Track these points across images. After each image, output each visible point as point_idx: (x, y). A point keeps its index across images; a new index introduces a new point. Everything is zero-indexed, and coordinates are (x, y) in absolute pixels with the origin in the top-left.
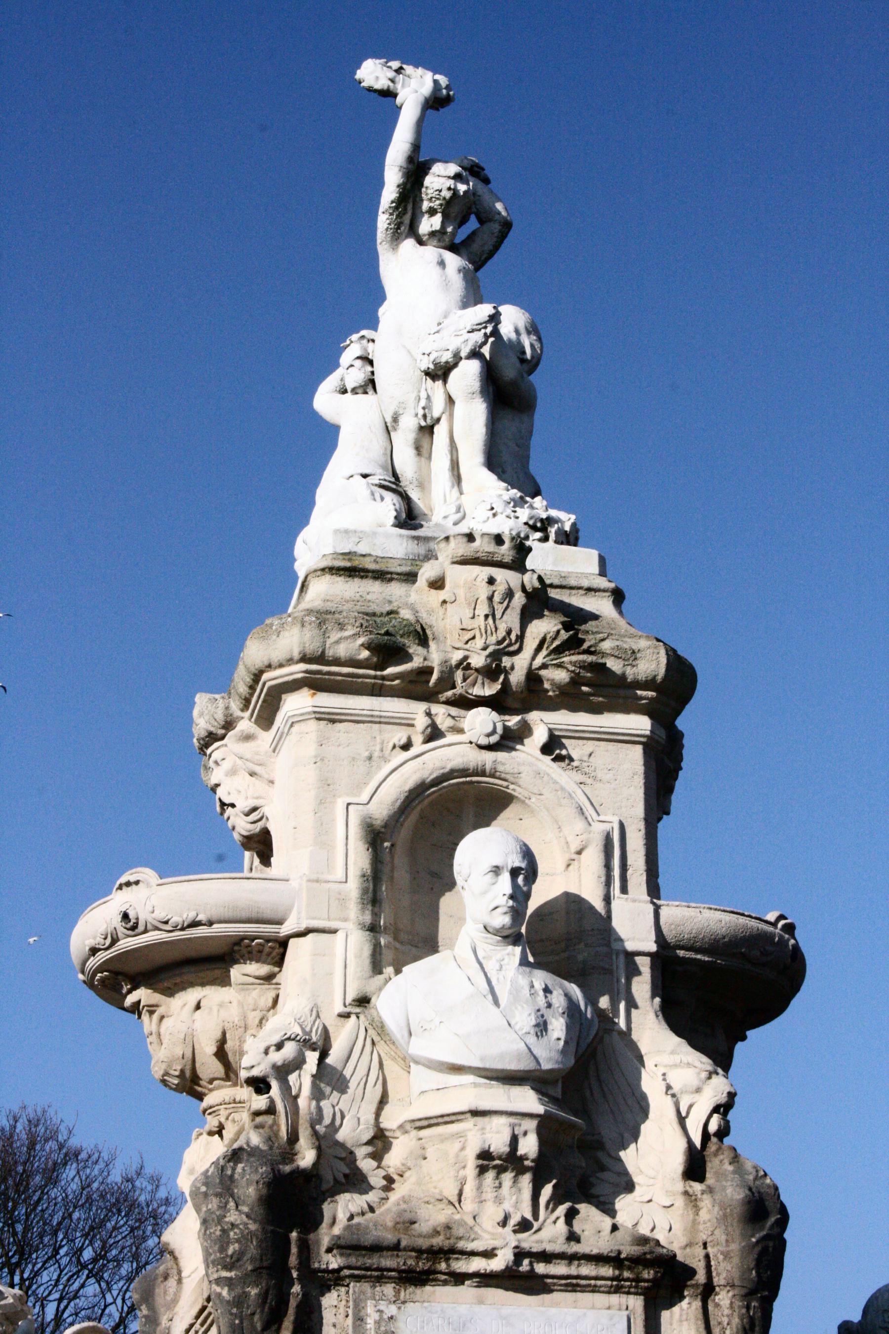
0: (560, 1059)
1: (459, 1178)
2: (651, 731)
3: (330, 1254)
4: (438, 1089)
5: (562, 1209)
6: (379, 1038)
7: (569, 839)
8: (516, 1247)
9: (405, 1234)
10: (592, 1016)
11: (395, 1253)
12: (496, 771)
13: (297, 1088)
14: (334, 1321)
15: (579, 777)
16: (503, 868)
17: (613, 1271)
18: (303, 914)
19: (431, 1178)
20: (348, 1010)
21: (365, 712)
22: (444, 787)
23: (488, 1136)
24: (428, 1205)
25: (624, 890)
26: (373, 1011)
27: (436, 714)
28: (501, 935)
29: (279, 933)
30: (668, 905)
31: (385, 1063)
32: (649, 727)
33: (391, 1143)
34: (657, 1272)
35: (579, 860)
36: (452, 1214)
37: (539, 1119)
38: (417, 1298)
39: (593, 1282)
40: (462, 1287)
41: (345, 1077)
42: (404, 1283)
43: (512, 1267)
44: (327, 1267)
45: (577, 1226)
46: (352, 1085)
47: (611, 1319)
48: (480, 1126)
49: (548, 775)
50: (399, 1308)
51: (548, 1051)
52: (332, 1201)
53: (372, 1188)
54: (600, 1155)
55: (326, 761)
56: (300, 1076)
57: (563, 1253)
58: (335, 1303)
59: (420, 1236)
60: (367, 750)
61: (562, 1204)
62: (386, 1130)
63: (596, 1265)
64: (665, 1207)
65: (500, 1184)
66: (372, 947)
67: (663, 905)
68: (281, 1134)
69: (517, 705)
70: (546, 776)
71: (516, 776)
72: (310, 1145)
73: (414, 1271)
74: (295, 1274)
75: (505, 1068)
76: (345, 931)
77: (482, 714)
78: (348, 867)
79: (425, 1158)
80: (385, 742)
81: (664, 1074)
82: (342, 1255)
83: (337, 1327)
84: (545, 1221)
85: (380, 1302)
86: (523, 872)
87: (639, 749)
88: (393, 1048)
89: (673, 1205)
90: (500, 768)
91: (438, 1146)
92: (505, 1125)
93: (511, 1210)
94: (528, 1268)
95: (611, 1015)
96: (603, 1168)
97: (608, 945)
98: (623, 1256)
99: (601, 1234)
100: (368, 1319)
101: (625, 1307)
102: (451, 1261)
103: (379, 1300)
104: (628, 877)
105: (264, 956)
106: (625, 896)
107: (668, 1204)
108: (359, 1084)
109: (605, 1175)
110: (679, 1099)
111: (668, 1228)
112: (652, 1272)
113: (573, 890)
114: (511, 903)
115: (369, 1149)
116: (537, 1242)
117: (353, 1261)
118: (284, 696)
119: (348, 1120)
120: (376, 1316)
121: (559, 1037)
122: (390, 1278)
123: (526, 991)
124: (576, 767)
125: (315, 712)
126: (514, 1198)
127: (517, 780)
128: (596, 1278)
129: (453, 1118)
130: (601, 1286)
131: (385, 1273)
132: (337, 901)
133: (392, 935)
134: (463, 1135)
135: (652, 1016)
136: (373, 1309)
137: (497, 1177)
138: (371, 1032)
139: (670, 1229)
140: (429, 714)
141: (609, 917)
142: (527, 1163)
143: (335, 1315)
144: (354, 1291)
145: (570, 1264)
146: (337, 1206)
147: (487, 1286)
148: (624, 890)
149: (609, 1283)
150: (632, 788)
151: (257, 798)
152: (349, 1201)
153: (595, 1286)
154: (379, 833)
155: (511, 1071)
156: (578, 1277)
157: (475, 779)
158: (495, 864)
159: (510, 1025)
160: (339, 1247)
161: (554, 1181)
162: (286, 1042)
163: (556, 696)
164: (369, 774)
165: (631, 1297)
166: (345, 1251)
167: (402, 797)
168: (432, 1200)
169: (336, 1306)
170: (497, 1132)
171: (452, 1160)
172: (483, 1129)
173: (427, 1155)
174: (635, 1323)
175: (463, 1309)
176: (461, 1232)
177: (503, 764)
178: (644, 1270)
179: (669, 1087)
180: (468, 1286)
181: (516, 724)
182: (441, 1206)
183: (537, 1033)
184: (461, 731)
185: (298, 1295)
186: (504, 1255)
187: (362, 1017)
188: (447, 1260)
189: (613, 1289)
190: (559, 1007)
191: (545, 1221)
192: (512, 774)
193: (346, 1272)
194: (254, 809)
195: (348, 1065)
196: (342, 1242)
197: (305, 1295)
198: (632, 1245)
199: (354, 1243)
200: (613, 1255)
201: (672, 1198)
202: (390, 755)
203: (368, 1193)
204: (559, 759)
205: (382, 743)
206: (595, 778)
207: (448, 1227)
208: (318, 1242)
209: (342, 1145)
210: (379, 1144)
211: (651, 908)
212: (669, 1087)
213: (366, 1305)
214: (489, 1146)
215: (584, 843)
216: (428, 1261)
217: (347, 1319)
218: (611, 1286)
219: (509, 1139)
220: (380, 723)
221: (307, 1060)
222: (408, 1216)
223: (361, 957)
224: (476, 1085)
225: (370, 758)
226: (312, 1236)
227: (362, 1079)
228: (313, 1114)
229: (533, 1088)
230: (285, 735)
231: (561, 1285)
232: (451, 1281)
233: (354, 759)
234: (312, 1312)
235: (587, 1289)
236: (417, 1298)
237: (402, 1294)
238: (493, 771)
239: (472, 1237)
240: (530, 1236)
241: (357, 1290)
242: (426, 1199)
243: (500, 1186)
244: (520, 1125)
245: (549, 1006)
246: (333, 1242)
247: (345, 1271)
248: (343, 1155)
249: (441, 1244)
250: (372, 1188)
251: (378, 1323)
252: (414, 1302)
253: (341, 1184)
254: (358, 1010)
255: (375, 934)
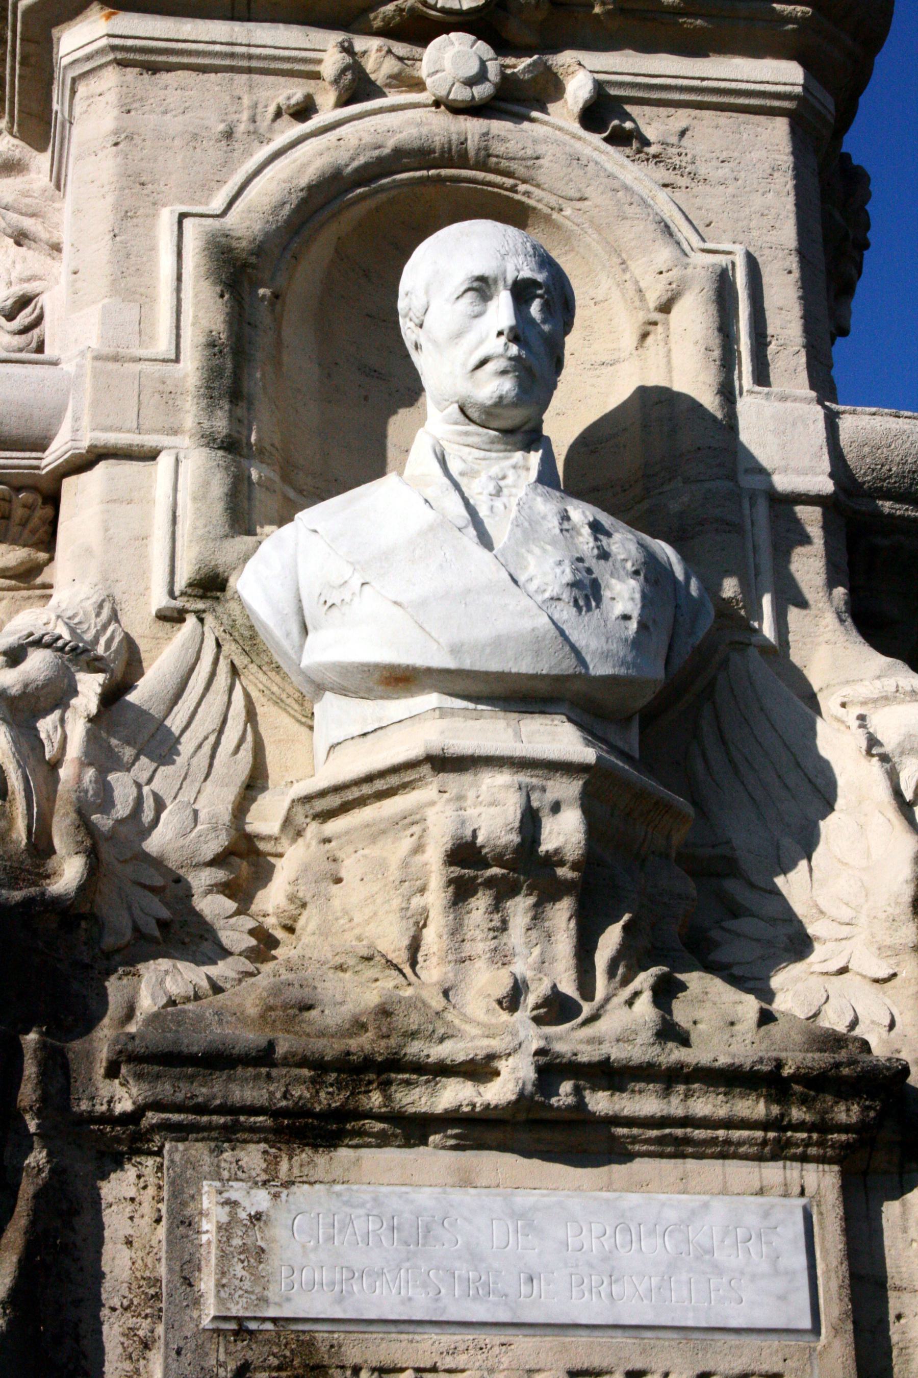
0: (629, 659)
1: (409, 913)
2: (804, 86)
3: (117, 1081)
4: (365, 735)
5: (644, 979)
6: (246, 660)
7: (643, 285)
8: (539, 1052)
9: (288, 1032)
10: (701, 595)
11: (264, 1070)
12: (489, 156)
13: (56, 745)
14: (130, 1231)
15: (662, 174)
16: (495, 281)
17: (767, 1108)
18: (86, 421)
19: (351, 920)
20: (179, 603)
21: (218, 48)
22: (383, 189)
23: (471, 812)
24: (341, 974)
25: (762, 376)
26: (233, 606)
27: (365, 52)
28: (496, 424)
29: (38, 468)
30: (854, 413)
31: (259, 710)
32: (801, 80)
33: (272, 867)
34: (869, 1108)
35: (667, 324)
36: (396, 987)
37: (586, 776)
38: (319, 1174)
39: (721, 1133)
40: (422, 1149)
41: (169, 731)
42: (287, 1142)
43: (532, 1095)
44: (110, 1110)
45: (681, 1013)
46: (186, 746)
47: (766, 1215)
48: (453, 791)
49: (597, 163)
50: (276, 1196)
51: (603, 639)
52: (126, 974)
53: (226, 953)
54: (732, 886)
55: (137, 140)
56: (62, 721)
57: (650, 1065)
58: (132, 1192)
59: (321, 1034)
60: (224, 121)
61: (645, 969)
62: (259, 837)
63: (725, 1094)
64: (876, 981)
65: (504, 922)
66: (229, 480)
67: (843, 412)
68: (14, 836)
69: (529, 38)
70: (591, 164)
71: (530, 163)
72: (72, 848)
73: (309, 1113)
74: (32, 1125)
75: (506, 670)
76: (174, 451)
77: (456, 44)
78: (182, 332)
79: (338, 881)
80: (260, 106)
81: (862, 718)
82: (139, 1077)
83: (135, 1245)
84: (607, 1000)
85: (231, 1183)
86: (540, 292)
87: (781, 125)
88: (277, 679)
89: (895, 975)
90: (498, 148)
91: (366, 851)
92: (508, 787)
93: (529, 974)
94: (570, 1100)
95: (743, 612)
96: (735, 911)
97: (732, 477)
98: (787, 1072)
99: (737, 1028)
100: (204, 1221)
101: (797, 1190)
102: (393, 1088)
103: (228, 1180)
104: (769, 357)
105: (15, 530)
106: (766, 389)
107: (883, 973)
108: (200, 746)
109: (744, 925)
110: (898, 767)
111: (887, 1022)
112: (855, 1108)
113: (654, 379)
114: (514, 350)
115: (220, 875)
116: (591, 1041)
117: (165, 1090)
118: (55, 32)
119: (170, 813)
120: (222, 1214)
121: (627, 612)
122: (253, 1129)
123: (553, 523)
124: (654, 156)
125: (114, 48)
126: (536, 951)
127: (532, 172)
128: (729, 1124)
129: (394, 780)
130: (740, 1143)
131: (242, 1118)
132: (157, 396)
133: (277, 468)
134: (418, 817)
135: (830, 619)
136: (215, 1198)
137: (497, 906)
138: (229, 647)
139: (892, 1025)
140: (348, 49)
141: (730, 425)
142: (564, 872)
143: (131, 1218)
144: (172, 1161)
145: (667, 1093)
146: (140, 981)
147: (480, 1146)
148: (762, 376)
149: (759, 1134)
150: (770, 196)
151: (29, 280)
152: (167, 972)
153: (728, 1142)
154: (245, 265)
155: (518, 675)
156: (687, 1121)
157: (444, 172)
158: (477, 273)
159: (515, 582)
160: (134, 1058)
161: (626, 917)
162: (30, 650)
163: (608, 13)
164: (227, 165)
165: (811, 1167)
166: (146, 1068)
167: (295, 199)
168: (351, 962)
169: (132, 1200)
170: (493, 803)
171: (394, 873)
172: (460, 798)
173: (343, 874)
174: (823, 1239)
175: (425, 1197)
176: (414, 1021)
177: (504, 140)
178: (837, 1103)
179: (873, 742)
180: (435, 1147)
181: (525, 71)
182: (370, 972)
183: (576, 602)
184: (418, 85)
185: (40, 1171)
186: (514, 1070)
187: (209, 619)
188: (385, 1086)
189: (767, 1149)
190: (625, 560)
191: (607, 1000)
192: (523, 159)
193: (152, 1118)
194: (24, 302)
195: (176, 709)
196: (138, 1047)
197: (57, 1172)
198: (807, 1051)
199: (164, 1047)
200: (765, 1068)
201: (892, 961)
202: (270, 129)
203: (215, 963)
204: (619, 139)
205: (255, 106)
206: (693, 176)
207: (384, 1012)
208: (89, 1056)
209: (157, 863)
210: (244, 867)
211: (818, 413)
212: (873, 742)
213: (199, 1191)
214: (474, 831)
215: (674, 286)
216: (339, 1089)
217: (159, 1227)
218: (765, 1142)
219: (519, 816)
220: (250, 71)
221: (79, 688)
222: (295, 994)
223: (204, 497)
224: (443, 712)
225: (229, 135)
226: (76, 1045)
227: (206, 738)
228: (87, 791)
229: (570, 720)
230: (68, 125)
231: (648, 1141)
232: (396, 1136)
233: (195, 137)
234: (74, 1212)
235: (709, 1151)
236: (319, 1174)
237: (284, 1166)
238: (483, 153)
239: (441, 1031)
240: (573, 1029)
241: (177, 1157)
242: (338, 960)
243: (504, 927)
244: (544, 790)
245: (604, 555)
246: (118, 1048)
247: (149, 1114)
248: (159, 881)
249: (368, 1047)
250: (226, 953)
251: (225, 1229)
252: (311, 1184)
253: (153, 940)
254: (200, 605)
255: (238, 458)
